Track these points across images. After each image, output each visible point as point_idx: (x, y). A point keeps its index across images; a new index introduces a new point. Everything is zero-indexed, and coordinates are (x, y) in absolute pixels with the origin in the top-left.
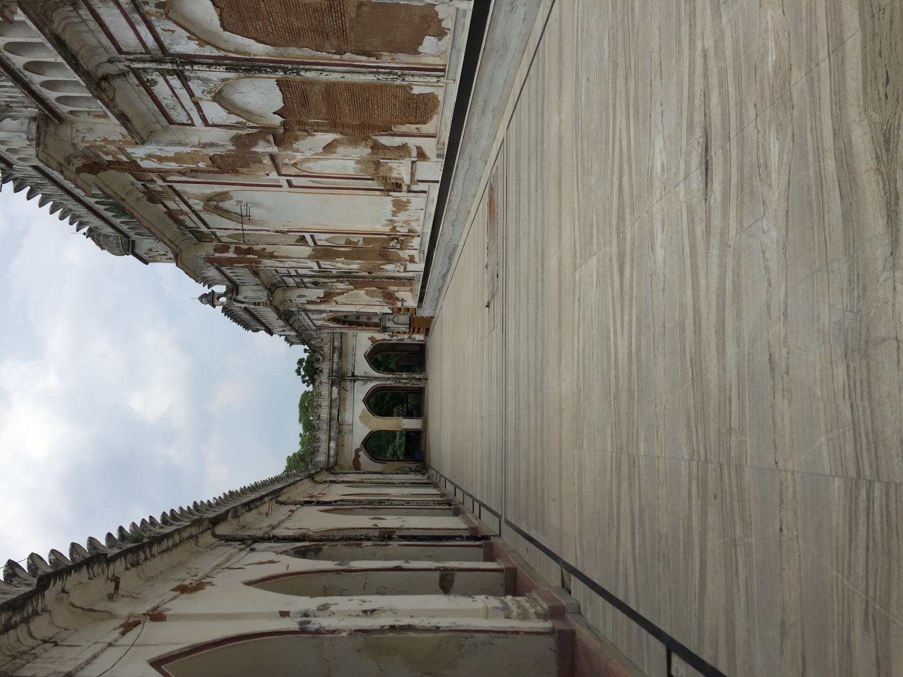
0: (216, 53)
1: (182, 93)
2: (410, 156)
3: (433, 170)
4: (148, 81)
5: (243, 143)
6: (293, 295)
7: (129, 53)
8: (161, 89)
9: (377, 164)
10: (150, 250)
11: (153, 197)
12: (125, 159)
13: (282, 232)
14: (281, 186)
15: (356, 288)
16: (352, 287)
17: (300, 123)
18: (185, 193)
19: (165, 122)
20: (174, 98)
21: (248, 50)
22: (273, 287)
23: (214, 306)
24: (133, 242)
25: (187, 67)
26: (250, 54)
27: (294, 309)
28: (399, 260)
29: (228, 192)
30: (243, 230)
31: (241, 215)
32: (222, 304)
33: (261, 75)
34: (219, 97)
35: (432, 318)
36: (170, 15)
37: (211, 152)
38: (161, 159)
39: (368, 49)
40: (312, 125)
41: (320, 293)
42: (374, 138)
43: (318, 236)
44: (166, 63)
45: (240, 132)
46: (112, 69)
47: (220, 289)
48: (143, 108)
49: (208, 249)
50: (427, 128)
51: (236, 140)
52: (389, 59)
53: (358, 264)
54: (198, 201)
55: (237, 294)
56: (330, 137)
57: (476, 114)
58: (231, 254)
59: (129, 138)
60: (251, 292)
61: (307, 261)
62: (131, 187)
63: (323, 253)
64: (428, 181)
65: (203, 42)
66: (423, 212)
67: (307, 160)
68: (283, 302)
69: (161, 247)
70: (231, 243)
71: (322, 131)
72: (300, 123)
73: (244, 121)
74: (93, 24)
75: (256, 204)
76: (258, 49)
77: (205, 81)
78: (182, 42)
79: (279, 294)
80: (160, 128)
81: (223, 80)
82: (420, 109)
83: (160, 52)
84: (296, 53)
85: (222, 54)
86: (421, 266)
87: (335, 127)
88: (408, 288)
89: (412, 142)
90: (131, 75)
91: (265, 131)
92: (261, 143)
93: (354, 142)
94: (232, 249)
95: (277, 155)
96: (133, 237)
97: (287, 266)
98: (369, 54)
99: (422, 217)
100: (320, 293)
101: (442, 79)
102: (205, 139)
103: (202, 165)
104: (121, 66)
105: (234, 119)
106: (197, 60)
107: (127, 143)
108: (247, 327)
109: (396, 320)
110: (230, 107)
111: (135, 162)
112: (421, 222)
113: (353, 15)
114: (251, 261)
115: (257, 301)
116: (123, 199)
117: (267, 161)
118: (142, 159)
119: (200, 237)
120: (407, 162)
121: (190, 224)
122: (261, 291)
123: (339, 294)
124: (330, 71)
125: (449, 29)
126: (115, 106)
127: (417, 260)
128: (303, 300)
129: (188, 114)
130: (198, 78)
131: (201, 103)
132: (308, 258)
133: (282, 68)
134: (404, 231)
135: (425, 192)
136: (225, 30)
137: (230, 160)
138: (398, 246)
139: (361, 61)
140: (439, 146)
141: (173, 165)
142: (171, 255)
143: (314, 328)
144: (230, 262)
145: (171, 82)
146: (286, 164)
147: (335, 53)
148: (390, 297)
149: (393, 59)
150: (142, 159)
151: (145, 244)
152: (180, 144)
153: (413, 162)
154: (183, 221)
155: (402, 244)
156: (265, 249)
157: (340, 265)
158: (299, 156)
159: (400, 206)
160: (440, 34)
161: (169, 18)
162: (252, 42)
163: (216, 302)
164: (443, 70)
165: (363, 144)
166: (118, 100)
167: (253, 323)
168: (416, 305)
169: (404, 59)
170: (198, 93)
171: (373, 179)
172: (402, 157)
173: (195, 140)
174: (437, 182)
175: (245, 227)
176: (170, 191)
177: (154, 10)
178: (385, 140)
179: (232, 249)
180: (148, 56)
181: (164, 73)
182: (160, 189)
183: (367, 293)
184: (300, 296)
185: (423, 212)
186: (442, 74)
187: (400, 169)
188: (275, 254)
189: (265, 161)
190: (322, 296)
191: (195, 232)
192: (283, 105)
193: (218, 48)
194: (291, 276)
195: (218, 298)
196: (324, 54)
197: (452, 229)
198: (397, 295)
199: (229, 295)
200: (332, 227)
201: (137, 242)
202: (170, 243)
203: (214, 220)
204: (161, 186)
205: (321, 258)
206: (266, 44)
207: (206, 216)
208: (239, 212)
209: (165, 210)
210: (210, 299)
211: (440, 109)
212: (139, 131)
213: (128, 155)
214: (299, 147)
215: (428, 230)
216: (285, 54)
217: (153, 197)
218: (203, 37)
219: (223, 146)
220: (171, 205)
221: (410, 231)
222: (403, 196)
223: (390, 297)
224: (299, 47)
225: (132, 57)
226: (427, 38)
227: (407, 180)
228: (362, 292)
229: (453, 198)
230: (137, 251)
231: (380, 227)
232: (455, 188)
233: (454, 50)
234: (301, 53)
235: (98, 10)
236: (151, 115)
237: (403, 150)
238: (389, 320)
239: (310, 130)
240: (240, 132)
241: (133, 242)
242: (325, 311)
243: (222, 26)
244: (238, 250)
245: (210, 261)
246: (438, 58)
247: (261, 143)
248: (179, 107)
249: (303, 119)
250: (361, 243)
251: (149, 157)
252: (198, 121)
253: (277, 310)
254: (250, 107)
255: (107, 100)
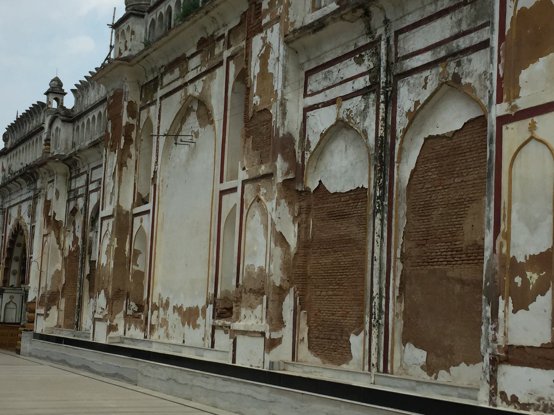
0: (399, 128)
1: (348, 89)
2: (271, 331)
3: (251, 355)
4: (362, 56)
5: (286, 145)
6: (60, 184)
7: (396, 41)
8: (350, 68)
9: (260, 292)
10: (133, 33)
11: (206, 44)
12: (264, 21)
13: (154, 179)
14: (221, 181)
15: (65, 259)
16: (67, 254)
17: (309, 208)
18: (212, 79)
19: (308, 67)
20: (339, 80)
21: (404, 160)
22: (72, 163)
23: (47, 93)
24: (143, 16)
25: (382, 97)
26: (399, 162)
27: (39, 185)
28: (112, 312)
29: (212, 122)
30: (158, 136)
31: (177, 135)
32: (50, 103)
33: (373, 172)
34: (342, 126)
35: (18, 352)
36: (445, 86)
37: (275, 110)
38: (264, 58)
39: (407, 287)
40: (307, 222)
41: (61, 216)
42: (292, 290)
43: (147, 221)
44: (386, 77)
45: (297, 143)
46: (377, 21)
47: (69, 102)
48: (327, 47)
49: (132, 95)
50: (303, 351)
51: (289, 138)
52: (396, 311)
53: (108, 264)
54: (200, 90)
55: (63, 121)
56: (292, 241)
57: (337, 409)
58: (125, 119)
59: (291, 29)
60: (64, 137)
61: (114, 204)
62: (221, 23)
63: (123, 224)
64: (234, 350)
65: (412, 116)
66: (181, 343)
67: (264, 213)
68: (51, 173)
69: (136, 45)
70: (139, 121)
71: (299, 231)
72: (309, 208)
73: (312, 149)
74: (431, 10)
75: (193, 152)
76: (404, 170)
77: (364, 114)
78: (412, 96)
79: (61, 168)
80: (302, 61)
81: (365, 132)
82: (330, 342)
83: (398, 71)
84: (401, 210)
85: (399, 134)
86: (101, 338)
87: (305, 247)
88: (61, 322)
89: (287, 333)
90: (369, 40)
91: (298, 171)
92: (286, 165)
93: (287, 267)
94: (134, 122)
95: (271, 181)
96: (149, 18)
97: (107, 180)
98: (402, 288)
99: (173, 341)
100: (61, 216)
101: (374, 370)
102: (290, 107)
103: (256, 100)
104: (380, 31)
105: (314, 139)
106: (390, 108)
107: (286, 25)
108: (12, 128)
109: (12, 305)
110: (328, 136)
111: (261, 31)
112: (166, 341)
113: (450, 274)
114: (116, 140)
115: (52, 143)
116: (207, 13)
117: (263, 169)
118: (264, 39)
119: (149, 88)
120: (263, 326)
121: (167, 79)
122: (66, 148)
123: (58, 239)
124: (381, 245)
125: (436, 378)
126: (334, 19)
127: (112, 334)
128: (51, 195)
129: (319, 92)
130: (367, 107)
131: (333, 107)
132: (118, 206)
133: (383, 194)
134: (153, 319)
135: (213, 346)
136: (426, 139)
137: (263, 129)
138: (130, 312)
139: (394, 279)
140: (282, 364)
141: (255, 69)
142: (126, 54)
143: (6, 206)
144: (115, 118)
145: (361, 79)
146: (258, 190)
147: (402, 252)
148: (50, 300)
149: (397, 315)
150: (264, 39)
151: (140, 28)
152: (285, 79)
153: (263, 334)
154: (172, 72)
155: (133, 316)
156: (131, 157)
157: (106, 242)
158: (270, 205)
159: (190, 316)
160: (430, 368)
161: (441, 85)
162: (413, 166)
163: (52, 96)
164: (385, 370)
165: (285, 277)
166: (340, 24)
167: (18, 136)
168: (38, 330)
169: (397, 326)
170: (346, 105)
171: (237, 286)
172: (270, 321)
173: (289, 96)
174: (234, 361)
175: (162, 140)
176: (215, 62)
177: (451, 71)
178: (289, 302)
179: (134, 122)
180: (393, 59)
181: (374, 73)
182: (217, 51)
183: (58, 272)
184: (57, 193)
185: (181, 343)
186: (381, 369)
187: (252, 318)
188: (124, 168)
189: (263, 167)
190: (57, 218)
191: (155, 83)
192: (332, 191)
193: (405, 131)
194: (87, 184)
195: (56, 99)
196: (401, 241)
197: (164, 378)
198: (54, 309)
199: (62, 112)
200: (160, 237)
201: (142, 20)
202: (143, 56)
203: (174, 104)
204: (221, 54)
205: (118, 220)
206: (410, 180)
207: (178, 97)
208: (183, 133)
209: (188, 55)
210: (56, 89)
211: (329, 366)
212: (300, 40)
213: (270, 25)
214: (282, 206)
215: (155, 349)
216: (400, 200)
217: (206, 44)
218: (418, 117)
219: (283, 124)
220: (195, 62)
221: (152, 327)
222: (207, 320)
223: (50, 300)
224: (407, 215)
225: (392, 42)
226: (425, 353)
227: (238, 326)
228: (59, 266)
229: (212, 380)
230: (131, 20)
231: (159, 291)
232: (228, 383)
233: (414, 384)
234: (401, 216)
235: (448, 18)
236: (318, 54)
237: (277, 322)
238: (11, 297)
239: (299, 217)
240: (297, 143)
241: (143, 16)
242: (33, 220)
243: (431, 137)
244: (130, 127)
245: (118, 95)
246: (399, 365)
247: (286, 165)
248: (326, 84)
249: (313, 212)
250: (136, 268)
251: (268, 47)
252: (310, 101)
253: (41, 164)
254: (327, 158)
255: (343, 12)
